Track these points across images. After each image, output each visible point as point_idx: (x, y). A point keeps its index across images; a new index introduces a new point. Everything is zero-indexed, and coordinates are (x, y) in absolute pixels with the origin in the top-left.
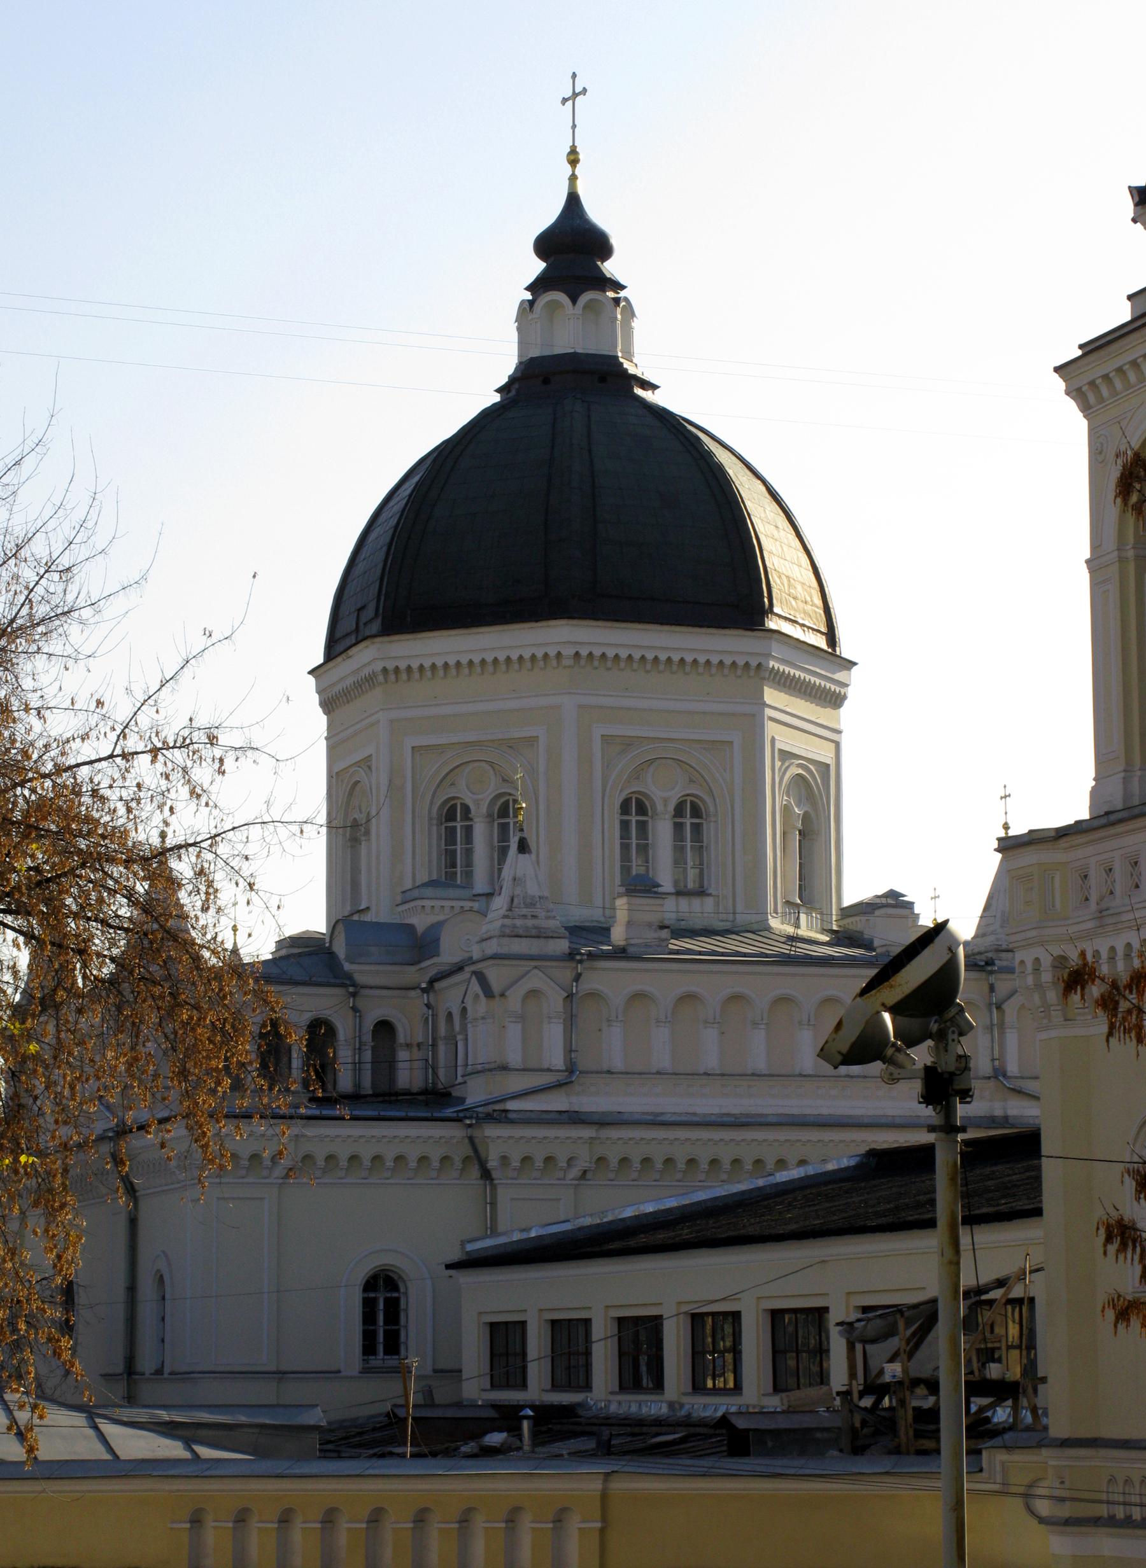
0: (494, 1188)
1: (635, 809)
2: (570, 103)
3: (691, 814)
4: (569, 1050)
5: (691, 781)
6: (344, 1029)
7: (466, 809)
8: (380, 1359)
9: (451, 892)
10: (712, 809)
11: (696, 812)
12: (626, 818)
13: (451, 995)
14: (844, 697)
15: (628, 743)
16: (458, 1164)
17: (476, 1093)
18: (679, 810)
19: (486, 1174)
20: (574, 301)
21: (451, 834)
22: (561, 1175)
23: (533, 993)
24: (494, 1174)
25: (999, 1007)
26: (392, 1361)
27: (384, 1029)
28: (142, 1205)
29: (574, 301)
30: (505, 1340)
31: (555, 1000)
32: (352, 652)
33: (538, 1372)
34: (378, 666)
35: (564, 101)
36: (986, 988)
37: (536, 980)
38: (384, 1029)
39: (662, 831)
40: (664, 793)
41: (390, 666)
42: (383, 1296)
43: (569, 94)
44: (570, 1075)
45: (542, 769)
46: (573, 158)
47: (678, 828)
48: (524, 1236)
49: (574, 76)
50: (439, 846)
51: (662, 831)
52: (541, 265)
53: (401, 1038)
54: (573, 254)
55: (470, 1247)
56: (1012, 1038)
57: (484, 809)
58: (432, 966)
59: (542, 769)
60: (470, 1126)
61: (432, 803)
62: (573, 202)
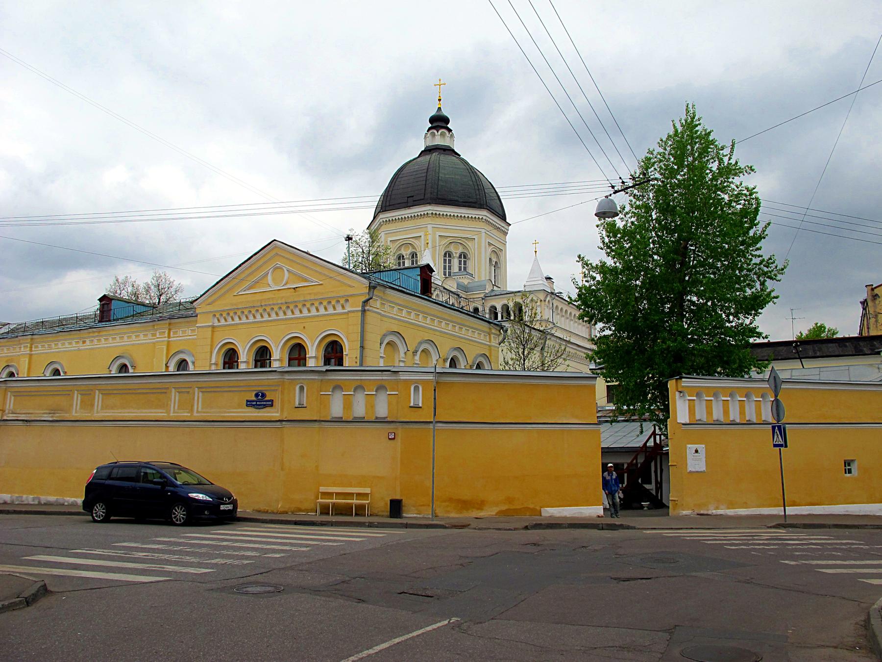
11: (465, 257)
18: (460, 257)
40: (456, 251)
52: (430, 125)
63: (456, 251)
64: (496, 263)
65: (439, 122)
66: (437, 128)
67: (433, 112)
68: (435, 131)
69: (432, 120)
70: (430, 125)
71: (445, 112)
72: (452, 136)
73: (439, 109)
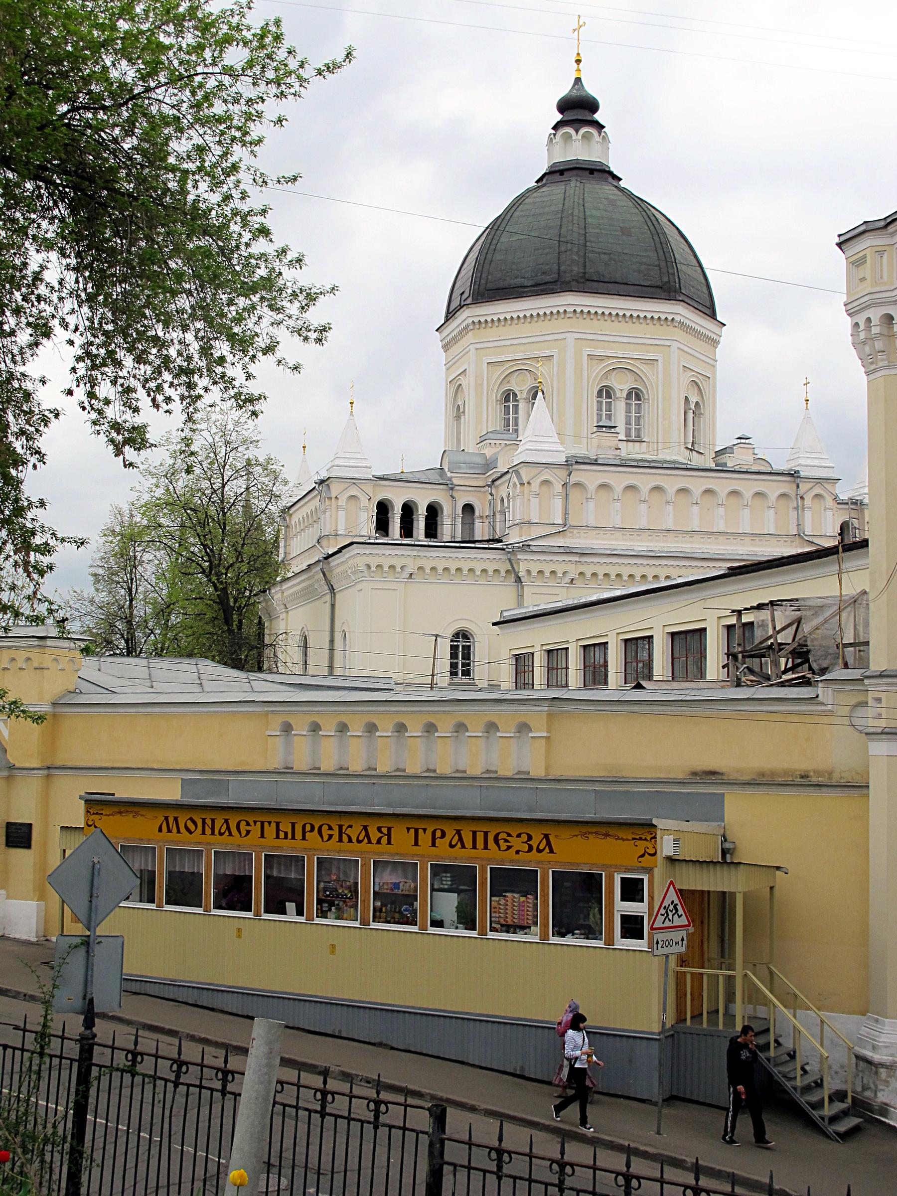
0: (522, 587)
1: (606, 392)
2: (576, 32)
3: (635, 395)
4: (566, 514)
5: (636, 380)
6: (447, 510)
7: (515, 395)
8: (460, 679)
9: (505, 436)
10: (646, 397)
11: (638, 398)
12: (600, 400)
13: (503, 491)
14: (718, 342)
15: (601, 358)
16: (503, 573)
17: (514, 538)
18: (629, 396)
19: (518, 580)
20: (577, 132)
21: (507, 408)
22: (559, 581)
23: (546, 482)
24: (523, 580)
25: (802, 498)
26: (466, 680)
27: (469, 509)
28: (337, 596)
29: (577, 132)
30: (522, 663)
31: (558, 487)
32: (456, 315)
33: (539, 675)
34: (470, 320)
35: (575, 30)
36: (795, 487)
37: (546, 475)
38: (469, 509)
39: (620, 407)
40: (621, 385)
41: (476, 320)
42: (462, 649)
43: (577, 26)
44: (564, 529)
45: (555, 373)
46: (578, 61)
47: (628, 405)
48: (536, 608)
49: (579, 16)
50: (500, 415)
51: (620, 407)
52: (559, 117)
53: (477, 513)
54: (578, 110)
55: (505, 614)
56: (808, 514)
57: (524, 396)
58: (493, 474)
59: (555, 373)
60: (509, 552)
61: (497, 392)
62: (578, 80)
63: (621, 385)
64: (697, 404)
65: (578, 110)
66: (577, 123)
67: (564, 89)
68: (571, 130)
69: (564, 106)
70: (559, 117)
71: (591, 89)
72: (605, 139)
73: (578, 80)
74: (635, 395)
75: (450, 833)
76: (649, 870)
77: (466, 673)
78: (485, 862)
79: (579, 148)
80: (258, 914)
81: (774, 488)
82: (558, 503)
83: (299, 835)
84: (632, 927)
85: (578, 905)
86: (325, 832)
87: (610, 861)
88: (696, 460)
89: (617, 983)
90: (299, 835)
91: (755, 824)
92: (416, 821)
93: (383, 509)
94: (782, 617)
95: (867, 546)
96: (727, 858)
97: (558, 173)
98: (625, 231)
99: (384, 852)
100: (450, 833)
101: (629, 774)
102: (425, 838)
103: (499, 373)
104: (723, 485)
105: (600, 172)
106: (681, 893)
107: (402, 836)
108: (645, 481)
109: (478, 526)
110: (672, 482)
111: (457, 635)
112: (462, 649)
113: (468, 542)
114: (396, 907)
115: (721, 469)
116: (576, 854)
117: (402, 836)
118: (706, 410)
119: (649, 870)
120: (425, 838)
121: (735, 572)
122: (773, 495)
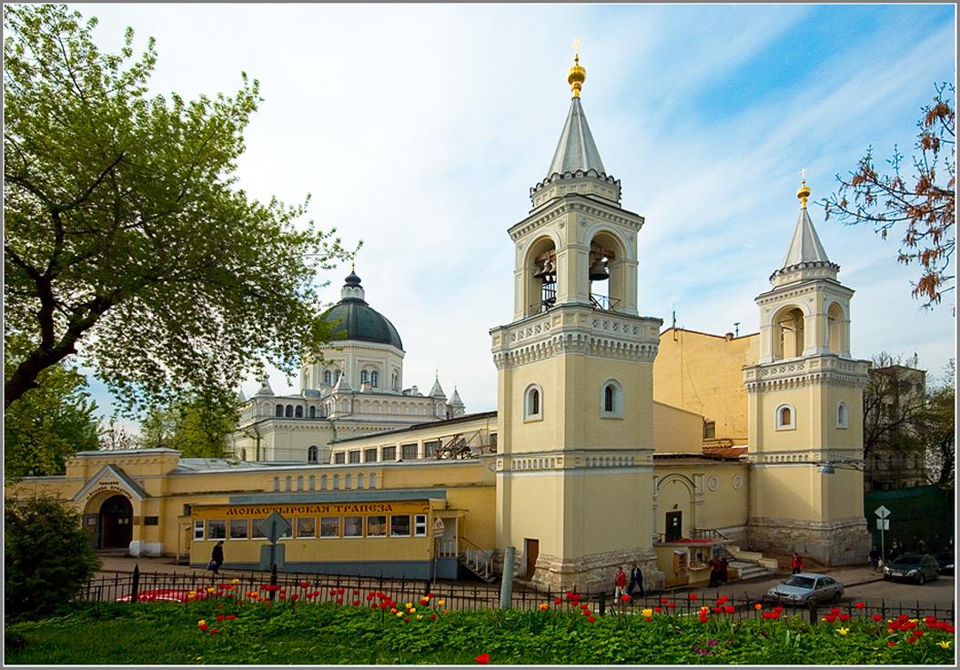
3: (375, 373)
4: (352, 410)
15: (362, 361)
19: (335, 430)
23: (345, 400)
31: (350, 401)
40: (370, 370)
42: (313, 453)
63: (370, 370)
67: (348, 274)
71: (358, 274)
74: (375, 373)
75: (352, 506)
76: (427, 513)
77: (315, 459)
78: (365, 514)
79: (353, 294)
80: (318, 537)
81: (426, 402)
82: (350, 406)
83: (290, 511)
84: (421, 530)
85: (401, 525)
86: (301, 510)
87: (412, 512)
88: (398, 394)
89: (415, 548)
90: (290, 511)
91: (455, 498)
92: (338, 505)
93: (279, 407)
94: (95, 463)
95: (496, 416)
96: (447, 507)
97: (345, 301)
98: (372, 322)
99: (326, 514)
100: (352, 506)
101: (411, 486)
102: (342, 510)
103: (362, 364)
104: (408, 401)
105: (361, 302)
106: (442, 519)
107: (333, 510)
108: (381, 399)
109: (316, 413)
110: (391, 400)
111: (310, 448)
112: (313, 453)
113: (313, 418)
114: (328, 530)
115: (405, 396)
116: (399, 510)
117: (333, 510)
118: (399, 379)
119: (427, 513)
120: (342, 510)
121: (411, 429)
122: (425, 404)
